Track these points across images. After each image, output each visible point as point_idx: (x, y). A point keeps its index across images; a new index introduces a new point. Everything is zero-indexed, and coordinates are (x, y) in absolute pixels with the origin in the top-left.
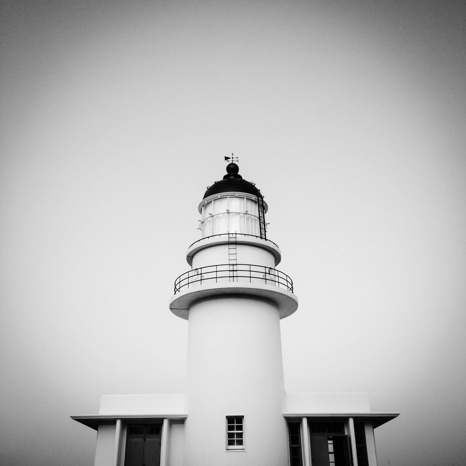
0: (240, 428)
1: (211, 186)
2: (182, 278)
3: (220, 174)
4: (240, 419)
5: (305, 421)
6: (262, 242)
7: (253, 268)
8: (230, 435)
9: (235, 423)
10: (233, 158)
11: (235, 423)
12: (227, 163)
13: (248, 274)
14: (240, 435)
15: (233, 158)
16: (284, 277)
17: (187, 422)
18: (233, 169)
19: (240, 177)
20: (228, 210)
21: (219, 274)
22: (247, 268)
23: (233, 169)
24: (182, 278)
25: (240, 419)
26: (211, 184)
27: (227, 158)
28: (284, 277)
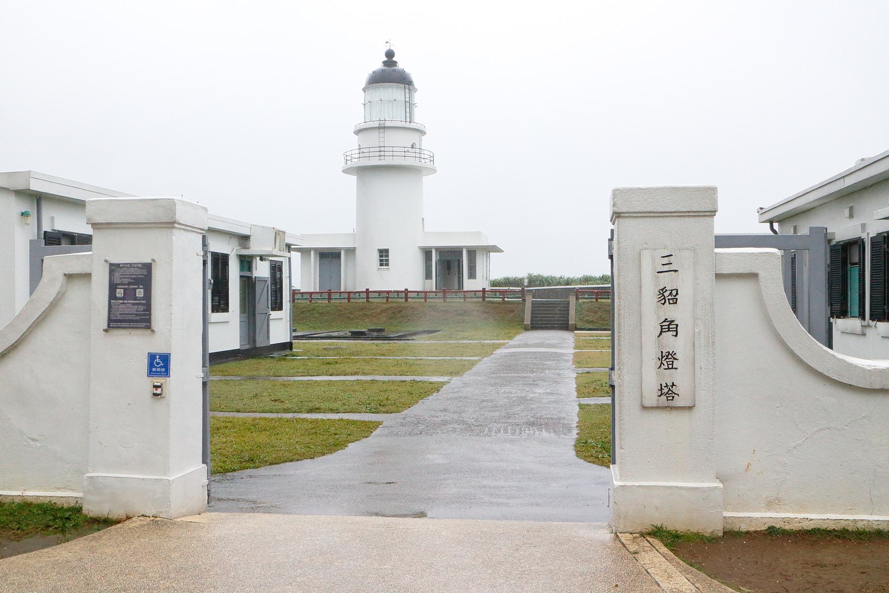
0: (387, 256)
4: (387, 251)
8: (381, 260)
9: (384, 254)
11: (384, 254)
13: (403, 154)
14: (388, 260)
17: (357, 251)
23: (390, 54)
25: (387, 251)
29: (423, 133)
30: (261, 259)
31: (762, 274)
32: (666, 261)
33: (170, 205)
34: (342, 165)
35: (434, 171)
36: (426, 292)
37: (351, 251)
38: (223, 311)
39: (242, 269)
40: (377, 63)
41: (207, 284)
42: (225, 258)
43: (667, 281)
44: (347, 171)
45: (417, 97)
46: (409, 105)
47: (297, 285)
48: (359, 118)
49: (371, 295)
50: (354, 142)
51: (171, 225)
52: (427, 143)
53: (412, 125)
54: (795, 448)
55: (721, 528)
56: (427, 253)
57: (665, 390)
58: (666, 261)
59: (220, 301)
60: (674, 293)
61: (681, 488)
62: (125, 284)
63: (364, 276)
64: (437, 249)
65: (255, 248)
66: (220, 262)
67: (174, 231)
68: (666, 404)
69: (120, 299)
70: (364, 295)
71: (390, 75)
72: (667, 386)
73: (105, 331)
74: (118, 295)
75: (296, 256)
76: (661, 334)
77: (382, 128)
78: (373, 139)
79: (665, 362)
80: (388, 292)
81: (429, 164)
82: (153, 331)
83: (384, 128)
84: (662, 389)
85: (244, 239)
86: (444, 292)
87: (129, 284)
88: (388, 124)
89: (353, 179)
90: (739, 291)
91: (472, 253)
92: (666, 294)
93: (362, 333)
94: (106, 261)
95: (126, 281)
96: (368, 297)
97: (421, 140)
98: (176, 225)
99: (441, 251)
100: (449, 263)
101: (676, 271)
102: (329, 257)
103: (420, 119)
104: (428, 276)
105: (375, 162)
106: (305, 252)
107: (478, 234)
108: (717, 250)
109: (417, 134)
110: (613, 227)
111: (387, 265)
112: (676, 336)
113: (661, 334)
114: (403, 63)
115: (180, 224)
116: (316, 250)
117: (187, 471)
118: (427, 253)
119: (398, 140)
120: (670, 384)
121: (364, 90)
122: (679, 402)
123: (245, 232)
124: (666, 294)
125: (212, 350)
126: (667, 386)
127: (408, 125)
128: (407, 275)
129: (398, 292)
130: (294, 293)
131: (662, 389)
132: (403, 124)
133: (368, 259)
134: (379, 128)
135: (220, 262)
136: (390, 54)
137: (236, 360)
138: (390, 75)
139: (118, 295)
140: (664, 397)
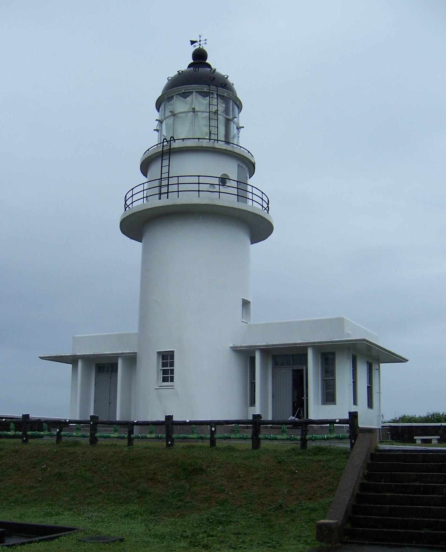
0: (172, 364)
1: (172, 76)
2: (135, 191)
3: (184, 62)
6: (229, 148)
7: (202, 180)
8: (165, 372)
10: (200, 41)
11: (167, 359)
12: (192, 49)
13: (196, 187)
15: (200, 41)
16: (260, 194)
18: (200, 57)
19: (209, 66)
20: (194, 109)
21: (202, 187)
22: (196, 180)
23: (200, 57)
24: (135, 191)
26: (173, 73)
27: (193, 42)
28: (260, 194)
111: (172, 380)
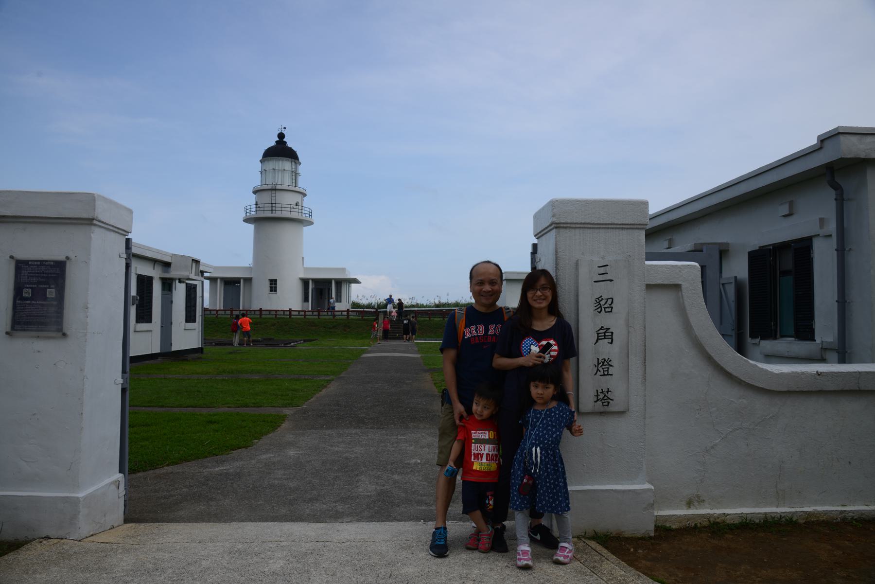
4: (275, 281)
5: (333, 283)
17: (254, 281)
23: (281, 136)
25: (275, 281)
29: (305, 195)
30: (180, 282)
31: (685, 285)
32: (602, 270)
33: (90, 199)
34: (243, 215)
35: (311, 223)
36: (305, 312)
37: (248, 281)
38: (147, 322)
39: (163, 289)
40: (272, 142)
41: (130, 301)
42: (150, 280)
43: (604, 290)
44: (247, 220)
45: (301, 169)
46: (295, 174)
47: (207, 305)
48: (257, 182)
49: (264, 313)
50: (252, 199)
51: (90, 222)
52: (307, 202)
53: (297, 189)
54: (712, 447)
55: (652, 527)
56: (305, 282)
57: (601, 396)
58: (602, 270)
59: (144, 315)
60: (610, 301)
61: (616, 491)
62: (34, 284)
63: (261, 300)
64: (313, 280)
65: (173, 273)
66: (145, 283)
67: (93, 227)
68: (602, 409)
69: (27, 299)
70: (258, 313)
71: (281, 151)
72: (603, 392)
73: (7, 333)
74: (25, 295)
75: (207, 283)
76: (597, 341)
77: (274, 190)
78: (266, 198)
79: (600, 369)
80: (276, 311)
81: (308, 218)
82: (64, 335)
83: (276, 190)
84: (598, 395)
85: (167, 265)
86: (319, 311)
87: (39, 283)
88: (278, 187)
89: (251, 227)
90: (663, 302)
91: (339, 283)
92: (602, 303)
93: (259, 341)
94: (12, 257)
95: (35, 280)
96: (261, 314)
97: (302, 200)
98: (95, 222)
99: (316, 281)
100: (321, 289)
101: (611, 280)
102: (231, 285)
103: (302, 184)
104: (306, 299)
105: (269, 214)
106: (213, 280)
107: (344, 270)
108: (648, 263)
109: (301, 196)
110: (536, 241)
111: (276, 291)
112: (611, 343)
113: (597, 341)
114: (290, 142)
115: (100, 221)
116: (222, 279)
117: (101, 481)
118: (305, 282)
119: (289, 199)
120: (605, 390)
121: (261, 161)
122: (613, 407)
123: (167, 259)
124: (602, 303)
125: (133, 353)
126: (603, 392)
127: (293, 188)
128: (290, 299)
129: (284, 311)
130: (205, 310)
131: (598, 395)
132: (290, 188)
133: (261, 287)
134: (272, 190)
135: (145, 283)
136: (281, 136)
137: (359, 521)
138: (281, 151)
139: (25, 295)
140: (599, 403)
